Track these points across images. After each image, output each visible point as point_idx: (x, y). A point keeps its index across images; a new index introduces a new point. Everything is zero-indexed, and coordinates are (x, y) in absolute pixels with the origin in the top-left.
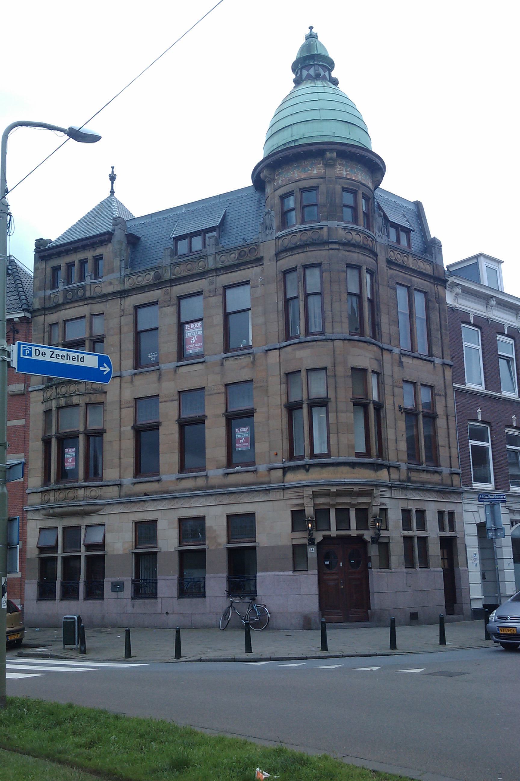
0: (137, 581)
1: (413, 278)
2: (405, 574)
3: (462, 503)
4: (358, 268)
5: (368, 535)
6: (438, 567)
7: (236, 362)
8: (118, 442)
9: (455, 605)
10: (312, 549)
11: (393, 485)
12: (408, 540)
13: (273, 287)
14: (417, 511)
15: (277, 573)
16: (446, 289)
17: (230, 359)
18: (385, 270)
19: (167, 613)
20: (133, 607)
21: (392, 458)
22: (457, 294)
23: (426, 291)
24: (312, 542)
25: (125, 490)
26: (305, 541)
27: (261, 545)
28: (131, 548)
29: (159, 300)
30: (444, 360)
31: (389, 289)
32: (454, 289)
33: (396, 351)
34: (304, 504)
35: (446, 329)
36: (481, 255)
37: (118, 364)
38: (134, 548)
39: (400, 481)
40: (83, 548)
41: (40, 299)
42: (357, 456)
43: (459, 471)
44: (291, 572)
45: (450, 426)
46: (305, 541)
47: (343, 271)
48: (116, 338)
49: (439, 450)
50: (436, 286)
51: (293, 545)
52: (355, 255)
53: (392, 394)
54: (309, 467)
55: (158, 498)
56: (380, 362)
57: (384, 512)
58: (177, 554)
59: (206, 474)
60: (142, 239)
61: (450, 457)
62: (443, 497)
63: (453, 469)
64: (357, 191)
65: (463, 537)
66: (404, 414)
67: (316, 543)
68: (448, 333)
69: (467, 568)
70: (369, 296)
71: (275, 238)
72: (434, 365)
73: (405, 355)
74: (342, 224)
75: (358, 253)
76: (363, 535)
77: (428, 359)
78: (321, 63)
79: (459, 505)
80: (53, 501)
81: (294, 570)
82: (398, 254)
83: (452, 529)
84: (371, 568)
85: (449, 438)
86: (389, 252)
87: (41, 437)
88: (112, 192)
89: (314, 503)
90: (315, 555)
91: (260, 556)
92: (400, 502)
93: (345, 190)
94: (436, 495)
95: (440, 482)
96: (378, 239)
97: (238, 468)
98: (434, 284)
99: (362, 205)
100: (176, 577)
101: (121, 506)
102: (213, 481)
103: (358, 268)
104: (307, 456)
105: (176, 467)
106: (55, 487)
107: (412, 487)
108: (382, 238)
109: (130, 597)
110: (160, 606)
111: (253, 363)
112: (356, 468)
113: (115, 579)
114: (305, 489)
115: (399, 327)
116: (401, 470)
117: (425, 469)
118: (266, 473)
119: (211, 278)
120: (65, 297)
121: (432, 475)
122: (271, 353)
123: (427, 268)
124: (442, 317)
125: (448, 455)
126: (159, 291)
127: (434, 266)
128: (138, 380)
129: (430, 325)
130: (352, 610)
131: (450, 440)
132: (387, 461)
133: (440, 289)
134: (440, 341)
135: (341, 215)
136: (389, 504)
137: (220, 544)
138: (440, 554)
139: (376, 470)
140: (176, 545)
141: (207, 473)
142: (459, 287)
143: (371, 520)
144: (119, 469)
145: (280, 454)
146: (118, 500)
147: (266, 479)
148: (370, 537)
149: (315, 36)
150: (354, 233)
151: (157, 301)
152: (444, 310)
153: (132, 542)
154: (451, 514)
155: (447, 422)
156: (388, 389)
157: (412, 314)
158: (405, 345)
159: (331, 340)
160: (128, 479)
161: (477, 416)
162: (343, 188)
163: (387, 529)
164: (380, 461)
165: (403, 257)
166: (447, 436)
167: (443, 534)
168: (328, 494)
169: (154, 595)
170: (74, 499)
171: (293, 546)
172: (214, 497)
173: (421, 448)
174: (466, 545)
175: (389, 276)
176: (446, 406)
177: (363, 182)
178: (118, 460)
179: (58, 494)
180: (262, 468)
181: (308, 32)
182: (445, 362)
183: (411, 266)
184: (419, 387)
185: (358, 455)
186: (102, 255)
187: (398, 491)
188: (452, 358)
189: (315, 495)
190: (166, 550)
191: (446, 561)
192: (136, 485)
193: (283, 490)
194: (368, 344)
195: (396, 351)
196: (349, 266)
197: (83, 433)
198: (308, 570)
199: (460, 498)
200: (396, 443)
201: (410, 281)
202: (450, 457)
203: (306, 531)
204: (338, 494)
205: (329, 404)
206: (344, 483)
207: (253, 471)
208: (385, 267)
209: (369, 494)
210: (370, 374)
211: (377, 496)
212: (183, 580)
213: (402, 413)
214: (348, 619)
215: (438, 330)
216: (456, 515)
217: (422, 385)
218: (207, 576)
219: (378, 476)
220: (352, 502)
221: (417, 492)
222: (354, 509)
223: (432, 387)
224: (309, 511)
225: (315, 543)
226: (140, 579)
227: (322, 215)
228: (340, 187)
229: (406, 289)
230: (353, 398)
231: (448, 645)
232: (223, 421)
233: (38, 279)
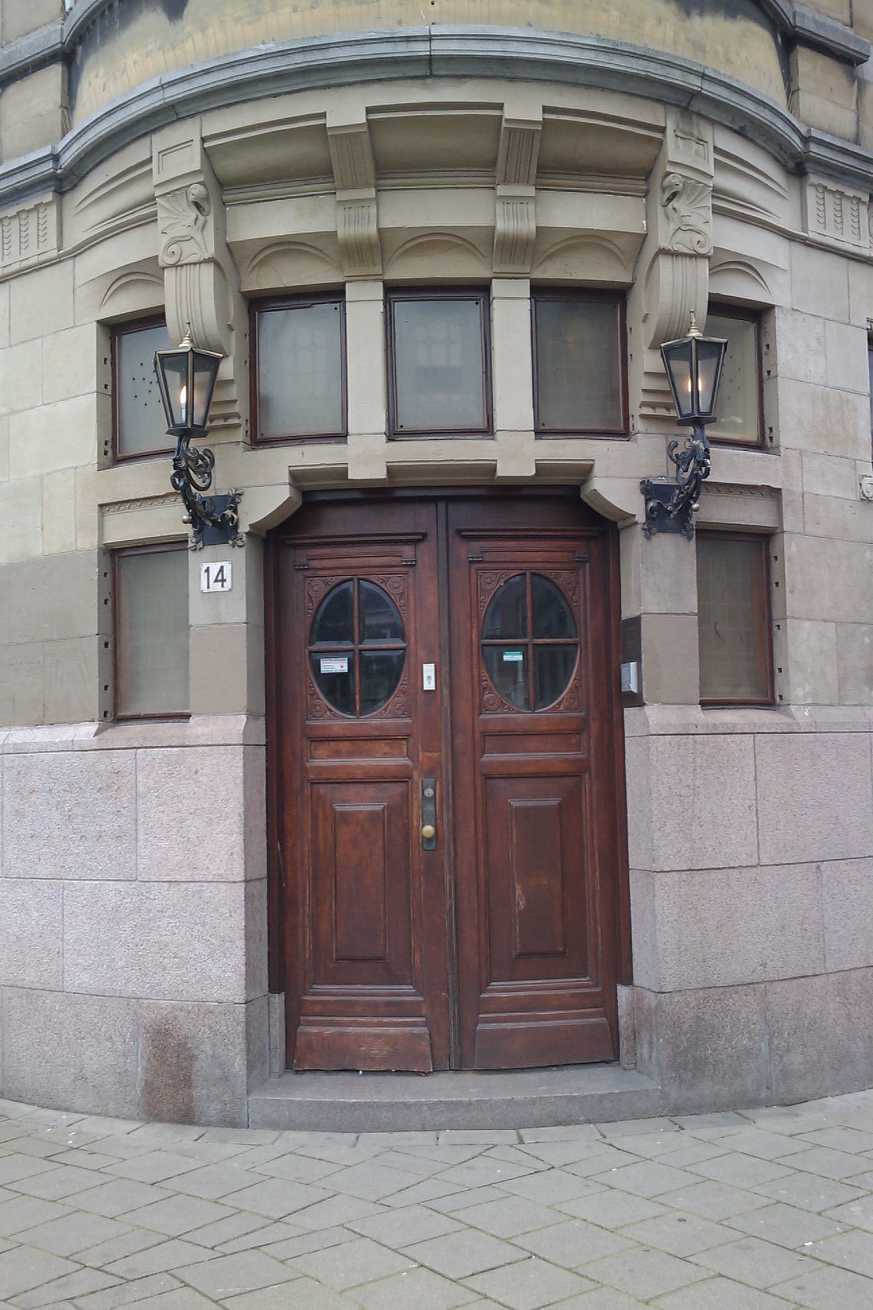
10: (215, 568)
42: (627, 153)
44: (86, 732)
67: (244, 528)
76: (586, 471)
84: (636, 700)
136: (781, 278)
148: (635, 485)
187: (846, 204)
220: (502, 226)
222: (523, 288)
225: (236, 527)
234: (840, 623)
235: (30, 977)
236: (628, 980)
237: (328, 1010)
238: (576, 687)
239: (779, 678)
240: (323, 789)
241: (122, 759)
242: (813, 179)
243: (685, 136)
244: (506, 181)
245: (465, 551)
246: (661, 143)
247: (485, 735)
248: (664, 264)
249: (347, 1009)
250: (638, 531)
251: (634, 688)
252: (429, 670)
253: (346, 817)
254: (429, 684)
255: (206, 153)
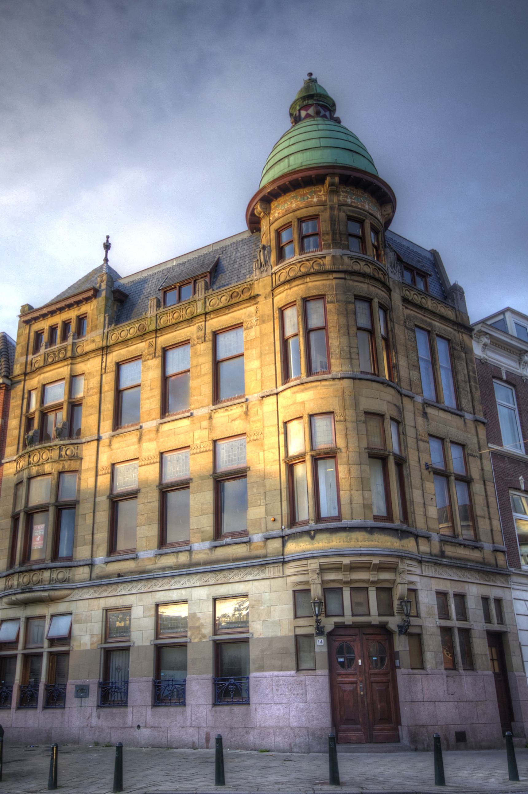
0: (105, 684)
1: (433, 322)
2: (445, 677)
3: (510, 588)
4: (368, 300)
5: (394, 622)
6: (487, 670)
7: (227, 413)
8: (92, 514)
9: (513, 723)
10: (320, 640)
11: (423, 559)
12: (446, 631)
13: (268, 327)
14: (455, 595)
15: (276, 673)
16: (472, 338)
17: (219, 410)
18: (401, 309)
19: (139, 727)
20: (99, 718)
21: (420, 524)
22: (485, 345)
23: (450, 338)
24: (320, 631)
25: (97, 571)
26: (311, 630)
27: (256, 636)
28: (100, 642)
29: (144, 353)
30: (476, 416)
31: (406, 330)
32: (482, 339)
33: (419, 399)
34: (309, 581)
35: (475, 382)
36: (508, 309)
37: (96, 427)
38: (103, 641)
39: (431, 554)
40: (46, 643)
41: (21, 365)
43: (505, 548)
44: (293, 672)
45: (489, 493)
46: (311, 630)
47: (350, 302)
48: (96, 398)
49: (477, 521)
50: (460, 334)
51: (296, 636)
52: (365, 286)
53: (416, 449)
54: (315, 534)
55: (133, 579)
56: (400, 410)
57: (413, 594)
58: (152, 648)
59: (189, 549)
60: (131, 296)
61: (492, 530)
62: (487, 579)
63: (496, 545)
64: (364, 220)
65: (516, 632)
66: (432, 473)
67: (326, 633)
68: (478, 386)
69: (523, 674)
70: (383, 333)
71: (270, 274)
72: (464, 421)
73: (429, 405)
74: (348, 252)
75: (368, 284)
76: (387, 623)
77: (458, 412)
78: (321, 103)
79: (507, 591)
80: (16, 587)
81: (298, 669)
82: (414, 294)
83: (501, 621)
84: (399, 667)
85: (488, 507)
86: (404, 291)
87: (10, 513)
88: (106, 260)
89: (322, 581)
90: (325, 649)
91: (254, 652)
92: (434, 581)
93: (350, 218)
94: (477, 577)
95: (481, 560)
96: (391, 275)
97: (228, 540)
98: (459, 331)
99: (371, 238)
100: (151, 678)
101: (91, 591)
102: (198, 557)
103: (368, 300)
104: (312, 520)
105: (155, 541)
106: (19, 570)
107: (447, 563)
108: (395, 274)
109: (96, 705)
110: (130, 717)
111: (246, 413)
112: (375, 534)
113: (79, 682)
114: (310, 561)
115: (420, 373)
116: (432, 542)
117: (462, 542)
118: (262, 544)
119: (199, 324)
120: (45, 360)
121: (471, 551)
122: (267, 400)
123: (450, 314)
124: (470, 368)
125: (489, 528)
126: (143, 344)
127: (457, 312)
128: (117, 443)
129: (456, 375)
130: (377, 727)
131: (490, 509)
132: (414, 529)
133: (466, 338)
134: (469, 395)
135: (346, 243)
137: (204, 636)
138: (488, 652)
139: (401, 539)
140: (152, 637)
141: (191, 547)
142: (488, 336)
143: (396, 603)
144: (90, 546)
145: (278, 518)
146: (88, 583)
147: (262, 552)
149: (315, 81)
150: (362, 264)
151: (141, 355)
152: (471, 361)
153: (102, 634)
154: (498, 602)
155: (485, 489)
156: (411, 442)
157: (435, 361)
158: (429, 393)
159: (338, 379)
160: (100, 557)
161: (520, 484)
162: (348, 216)
163: (418, 616)
164: (405, 527)
165: (420, 299)
166: (486, 504)
167: (490, 627)
168: (338, 568)
169: (124, 704)
170: (39, 583)
171: (296, 637)
172: (199, 576)
173: (503, 336)
174: (520, 643)
175: (405, 316)
176: (482, 469)
177: (370, 211)
178: (91, 535)
179: (22, 579)
180: (257, 538)
181: (308, 78)
182: (478, 419)
183: (430, 308)
184: (448, 444)
185: (376, 518)
186: (86, 313)
188: (485, 415)
189: (323, 570)
190: (140, 644)
191: (496, 663)
192: (109, 565)
193: (283, 564)
194: (385, 385)
195: (419, 399)
196: (359, 298)
197: (54, 504)
198: (315, 670)
199: (507, 581)
200: (425, 507)
201: (430, 325)
202: (492, 530)
203: (312, 617)
204: (352, 568)
205: (338, 455)
206: (360, 552)
207: (245, 543)
208: (401, 307)
209: (393, 569)
210: (387, 421)
211: (403, 572)
212: (160, 682)
213: (430, 472)
214: (371, 739)
215: (466, 382)
216: (505, 604)
217: (452, 442)
218: (188, 676)
219: (403, 546)
221: (454, 570)
222: (374, 589)
223: (463, 446)
224: (316, 591)
226: (111, 681)
227: (324, 244)
228: (344, 214)
229: (426, 333)
230: (368, 448)
231: (523, 781)
232: (210, 484)
233: (20, 345)
234: (435, 652)
235: (281, 724)
236: (401, 725)
237: (344, 731)
238: (387, 665)
239: (424, 664)
240: (340, 685)
241: (302, 678)
242: (423, 564)
243: (402, 562)
244: (372, 571)
245: (365, 637)
246: (398, 565)
247: (371, 674)
248: (399, 586)
249: (347, 730)
250: (397, 634)
251: (398, 665)
252: (360, 661)
253: (345, 691)
254: (360, 664)
255: (320, 565)
